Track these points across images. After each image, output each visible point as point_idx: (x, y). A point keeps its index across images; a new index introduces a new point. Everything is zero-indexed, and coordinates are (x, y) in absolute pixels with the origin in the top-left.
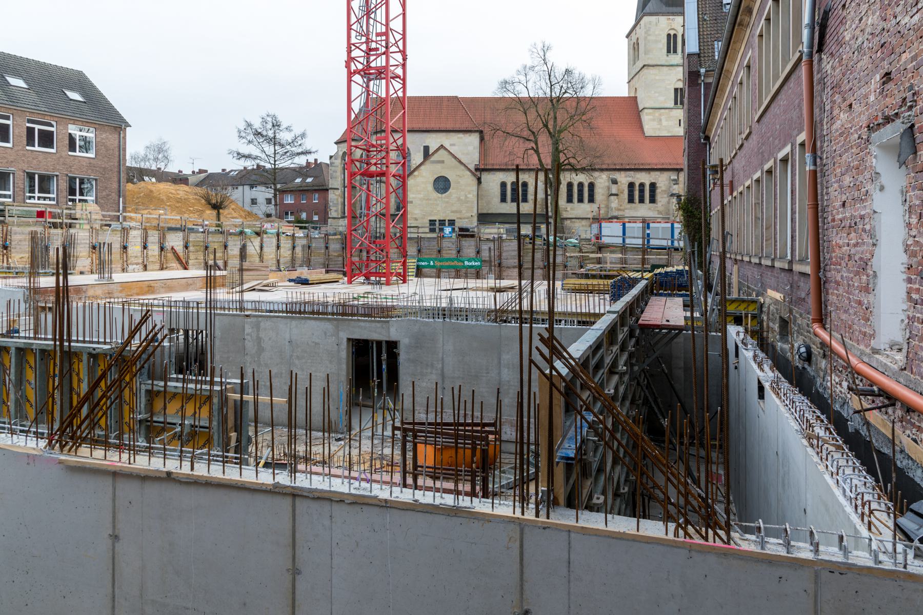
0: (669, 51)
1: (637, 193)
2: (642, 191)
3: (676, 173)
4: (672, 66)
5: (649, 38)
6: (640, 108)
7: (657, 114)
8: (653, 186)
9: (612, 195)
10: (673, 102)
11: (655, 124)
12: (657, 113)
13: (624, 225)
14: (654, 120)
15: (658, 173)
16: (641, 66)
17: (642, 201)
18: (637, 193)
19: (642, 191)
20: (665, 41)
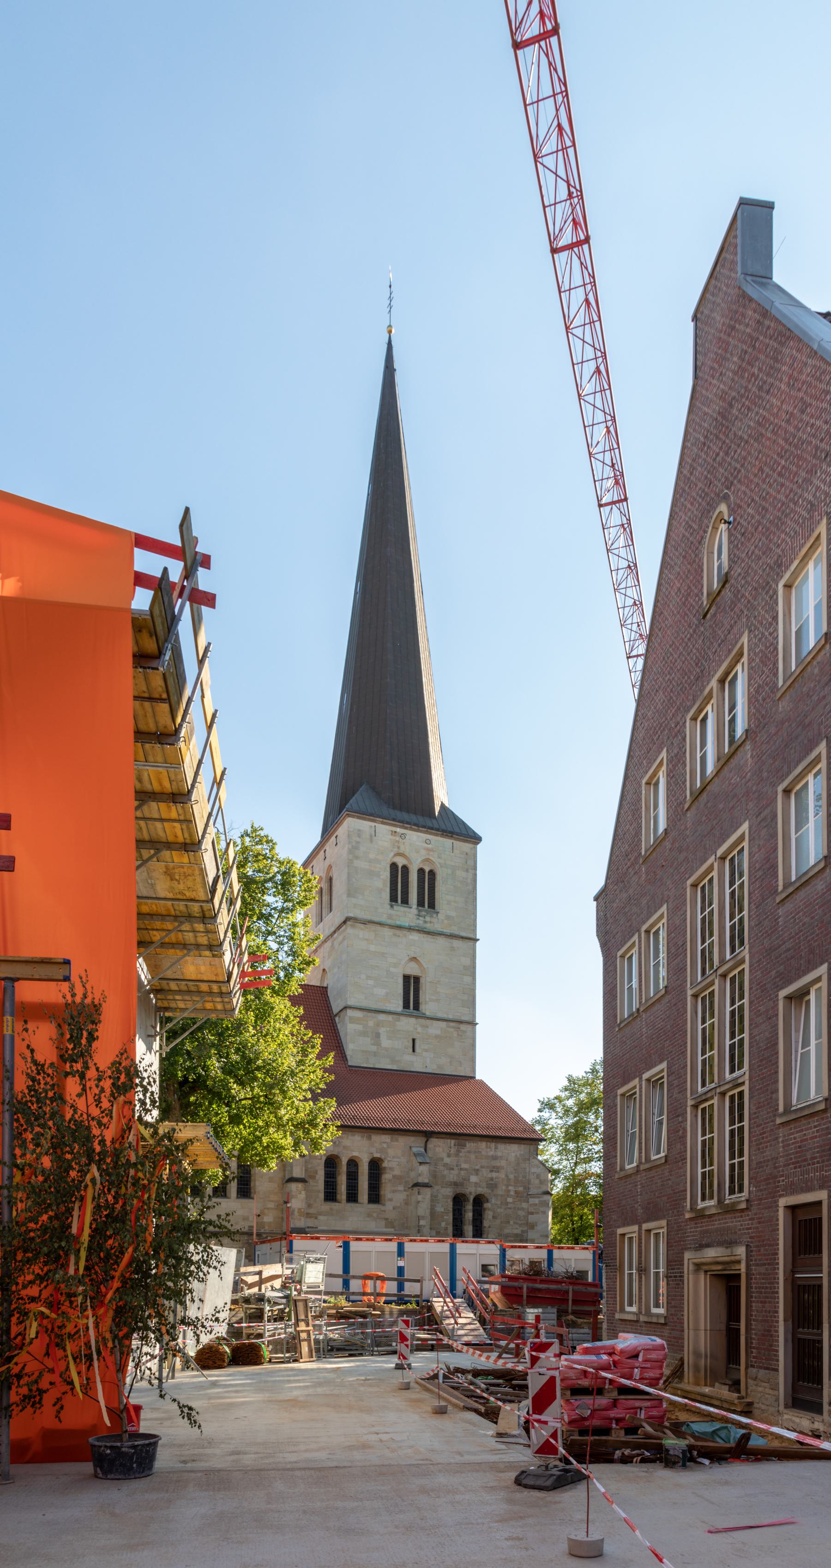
0: (393, 899)
1: (342, 1181)
2: (353, 1176)
3: (421, 1140)
4: (399, 927)
5: (356, 863)
6: (336, 1007)
7: (371, 1023)
8: (375, 1166)
9: (292, 1180)
10: (401, 1003)
11: (366, 1043)
12: (372, 1021)
13: (346, 1246)
14: (364, 1034)
15: (386, 1138)
16: (339, 920)
17: (352, 1197)
18: (342, 1181)
19: (353, 1176)
20: (386, 875)
